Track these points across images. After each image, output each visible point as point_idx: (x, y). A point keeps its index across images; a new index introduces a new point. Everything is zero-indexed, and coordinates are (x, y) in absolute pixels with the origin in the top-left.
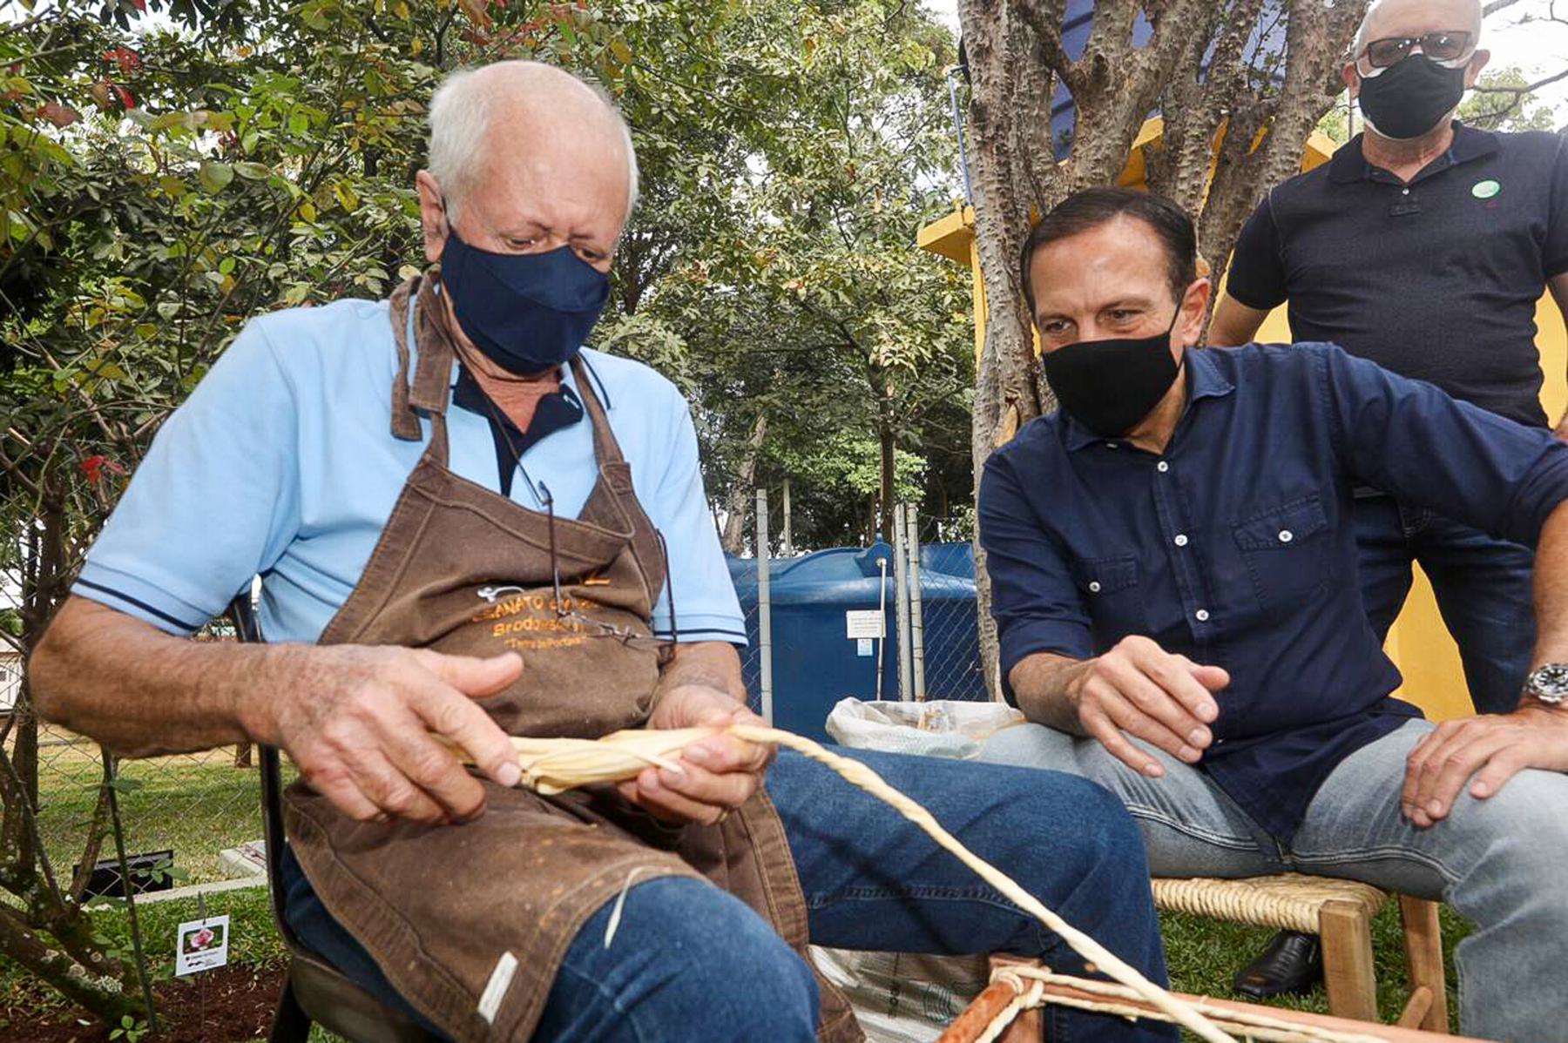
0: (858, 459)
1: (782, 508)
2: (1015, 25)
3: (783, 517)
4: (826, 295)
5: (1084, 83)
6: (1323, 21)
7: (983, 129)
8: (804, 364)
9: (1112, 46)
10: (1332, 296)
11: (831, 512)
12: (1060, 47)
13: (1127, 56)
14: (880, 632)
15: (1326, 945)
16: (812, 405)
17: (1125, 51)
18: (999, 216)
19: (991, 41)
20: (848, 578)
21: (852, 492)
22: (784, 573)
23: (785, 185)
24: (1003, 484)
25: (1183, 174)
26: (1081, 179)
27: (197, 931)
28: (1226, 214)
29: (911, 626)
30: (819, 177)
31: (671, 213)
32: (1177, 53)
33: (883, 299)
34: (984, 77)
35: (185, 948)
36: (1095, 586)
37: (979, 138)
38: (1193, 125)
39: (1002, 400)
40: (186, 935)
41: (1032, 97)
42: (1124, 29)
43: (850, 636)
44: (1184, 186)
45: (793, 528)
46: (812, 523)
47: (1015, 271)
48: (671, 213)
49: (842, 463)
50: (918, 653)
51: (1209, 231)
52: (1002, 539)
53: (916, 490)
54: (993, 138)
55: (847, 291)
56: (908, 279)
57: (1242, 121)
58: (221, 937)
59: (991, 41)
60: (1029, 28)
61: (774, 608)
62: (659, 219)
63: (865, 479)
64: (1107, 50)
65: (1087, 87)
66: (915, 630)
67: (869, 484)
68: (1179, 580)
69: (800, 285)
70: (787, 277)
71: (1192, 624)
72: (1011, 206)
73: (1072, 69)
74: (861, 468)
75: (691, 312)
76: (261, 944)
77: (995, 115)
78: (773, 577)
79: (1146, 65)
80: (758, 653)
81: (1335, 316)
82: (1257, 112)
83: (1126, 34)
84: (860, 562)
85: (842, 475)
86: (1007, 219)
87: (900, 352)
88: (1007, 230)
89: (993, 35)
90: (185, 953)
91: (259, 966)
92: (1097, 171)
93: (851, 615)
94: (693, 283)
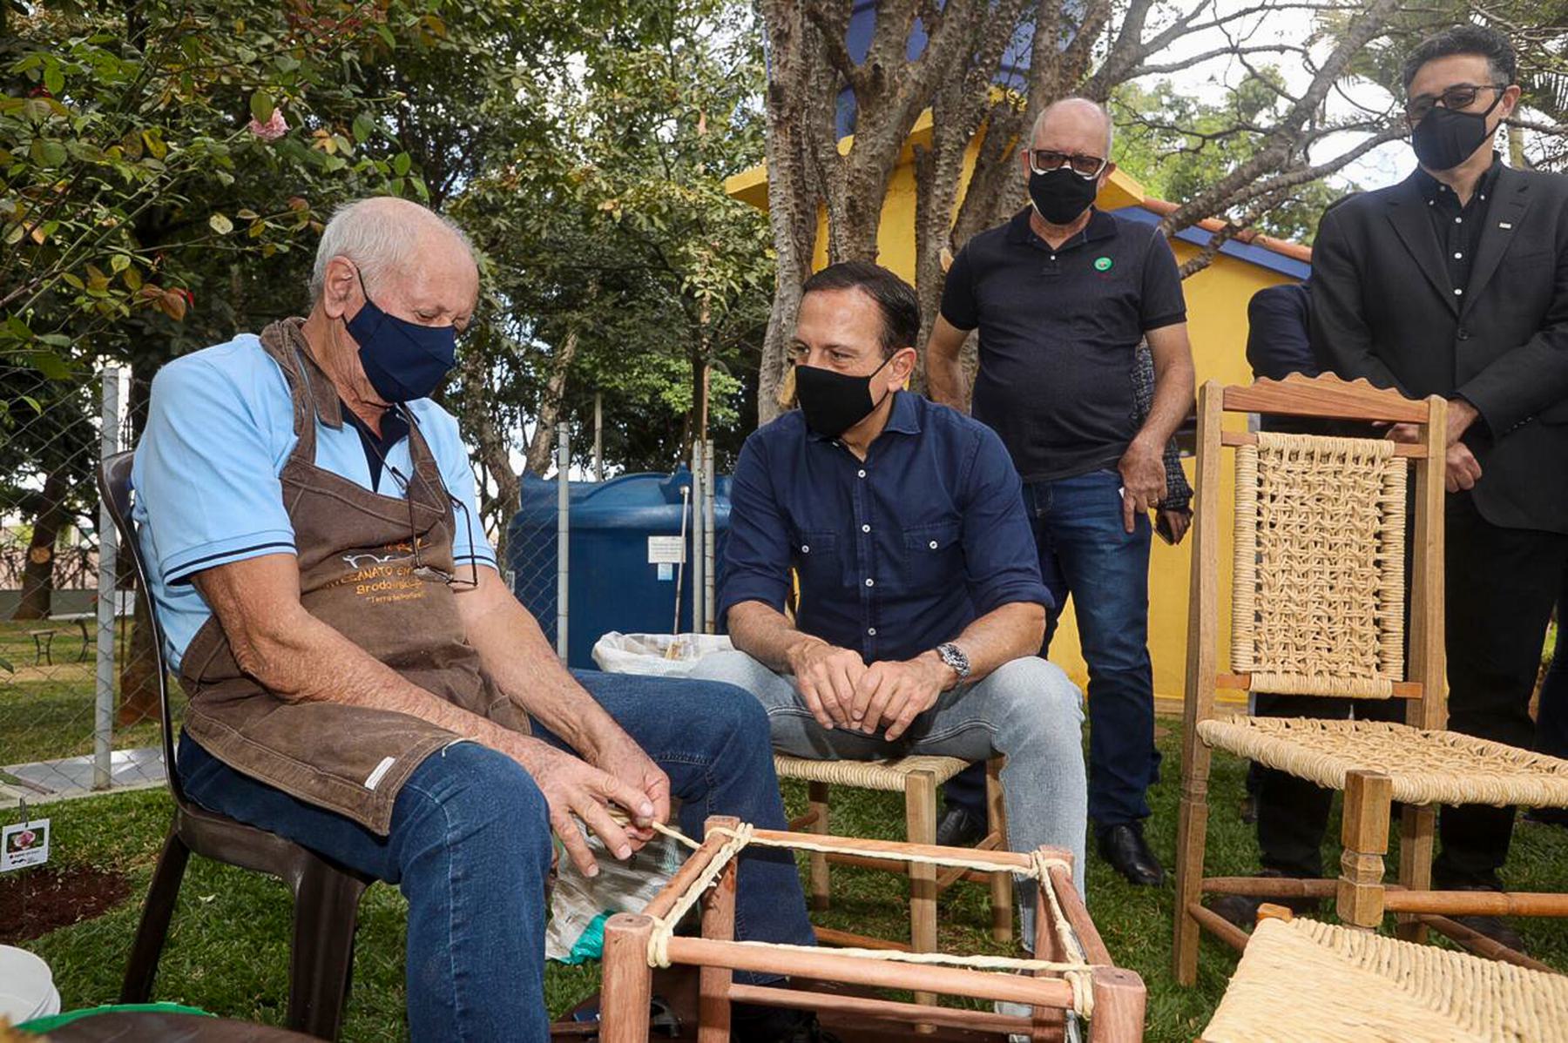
0: (673, 378)
1: (593, 422)
2: (808, 24)
3: (594, 431)
4: (642, 218)
5: (864, 86)
6: (1056, 62)
7: (779, 109)
8: (619, 282)
9: (889, 57)
10: (999, 330)
11: (645, 426)
12: (845, 51)
13: (901, 66)
14: (680, 558)
15: (907, 797)
16: (624, 328)
17: (900, 62)
18: (790, 192)
19: (790, 27)
20: (651, 504)
21: (666, 407)
22: (589, 497)
23: (604, 99)
24: (756, 461)
25: (938, 182)
26: (859, 171)
27: (20, 833)
28: (978, 213)
29: (704, 556)
30: (639, 96)
31: (482, 111)
32: (942, 71)
33: (700, 226)
34: (783, 60)
35: (8, 848)
36: (805, 549)
37: (775, 117)
38: (947, 140)
39: (784, 360)
40: (10, 836)
41: (819, 92)
42: (899, 44)
43: (650, 561)
44: (938, 192)
45: (604, 444)
46: (624, 438)
47: (801, 244)
48: (482, 111)
49: (654, 379)
50: (709, 581)
51: (964, 226)
52: (747, 505)
53: (730, 411)
54: (787, 119)
55: (663, 217)
56: (722, 213)
57: (997, 132)
58: (42, 838)
59: (790, 27)
60: (819, 31)
61: (572, 531)
62: (469, 116)
63: (678, 397)
64: (884, 59)
65: (867, 89)
66: (708, 560)
67: (683, 403)
68: (859, 554)
69: (616, 207)
70: (603, 198)
71: (861, 585)
72: (801, 183)
73: (854, 72)
74: (677, 386)
75: (500, 222)
76: (62, 852)
77: (790, 97)
78: (574, 500)
79: (916, 78)
80: (556, 579)
81: (1002, 346)
82: (1009, 125)
83: (901, 48)
84: (663, 489)
85: (656, 392)
86: (797, 195)
87: (712, 284)
88: (796, 205)
89: (792, 22)
90: (8, 852)
91: (62, 871)
92: (873, 165)
93: (652, 540)
94: (504, 190)
